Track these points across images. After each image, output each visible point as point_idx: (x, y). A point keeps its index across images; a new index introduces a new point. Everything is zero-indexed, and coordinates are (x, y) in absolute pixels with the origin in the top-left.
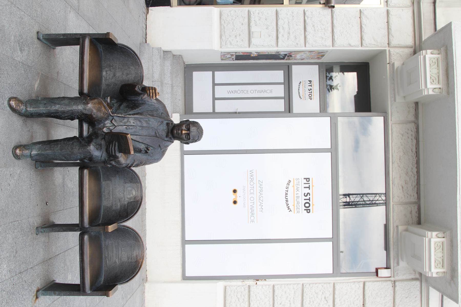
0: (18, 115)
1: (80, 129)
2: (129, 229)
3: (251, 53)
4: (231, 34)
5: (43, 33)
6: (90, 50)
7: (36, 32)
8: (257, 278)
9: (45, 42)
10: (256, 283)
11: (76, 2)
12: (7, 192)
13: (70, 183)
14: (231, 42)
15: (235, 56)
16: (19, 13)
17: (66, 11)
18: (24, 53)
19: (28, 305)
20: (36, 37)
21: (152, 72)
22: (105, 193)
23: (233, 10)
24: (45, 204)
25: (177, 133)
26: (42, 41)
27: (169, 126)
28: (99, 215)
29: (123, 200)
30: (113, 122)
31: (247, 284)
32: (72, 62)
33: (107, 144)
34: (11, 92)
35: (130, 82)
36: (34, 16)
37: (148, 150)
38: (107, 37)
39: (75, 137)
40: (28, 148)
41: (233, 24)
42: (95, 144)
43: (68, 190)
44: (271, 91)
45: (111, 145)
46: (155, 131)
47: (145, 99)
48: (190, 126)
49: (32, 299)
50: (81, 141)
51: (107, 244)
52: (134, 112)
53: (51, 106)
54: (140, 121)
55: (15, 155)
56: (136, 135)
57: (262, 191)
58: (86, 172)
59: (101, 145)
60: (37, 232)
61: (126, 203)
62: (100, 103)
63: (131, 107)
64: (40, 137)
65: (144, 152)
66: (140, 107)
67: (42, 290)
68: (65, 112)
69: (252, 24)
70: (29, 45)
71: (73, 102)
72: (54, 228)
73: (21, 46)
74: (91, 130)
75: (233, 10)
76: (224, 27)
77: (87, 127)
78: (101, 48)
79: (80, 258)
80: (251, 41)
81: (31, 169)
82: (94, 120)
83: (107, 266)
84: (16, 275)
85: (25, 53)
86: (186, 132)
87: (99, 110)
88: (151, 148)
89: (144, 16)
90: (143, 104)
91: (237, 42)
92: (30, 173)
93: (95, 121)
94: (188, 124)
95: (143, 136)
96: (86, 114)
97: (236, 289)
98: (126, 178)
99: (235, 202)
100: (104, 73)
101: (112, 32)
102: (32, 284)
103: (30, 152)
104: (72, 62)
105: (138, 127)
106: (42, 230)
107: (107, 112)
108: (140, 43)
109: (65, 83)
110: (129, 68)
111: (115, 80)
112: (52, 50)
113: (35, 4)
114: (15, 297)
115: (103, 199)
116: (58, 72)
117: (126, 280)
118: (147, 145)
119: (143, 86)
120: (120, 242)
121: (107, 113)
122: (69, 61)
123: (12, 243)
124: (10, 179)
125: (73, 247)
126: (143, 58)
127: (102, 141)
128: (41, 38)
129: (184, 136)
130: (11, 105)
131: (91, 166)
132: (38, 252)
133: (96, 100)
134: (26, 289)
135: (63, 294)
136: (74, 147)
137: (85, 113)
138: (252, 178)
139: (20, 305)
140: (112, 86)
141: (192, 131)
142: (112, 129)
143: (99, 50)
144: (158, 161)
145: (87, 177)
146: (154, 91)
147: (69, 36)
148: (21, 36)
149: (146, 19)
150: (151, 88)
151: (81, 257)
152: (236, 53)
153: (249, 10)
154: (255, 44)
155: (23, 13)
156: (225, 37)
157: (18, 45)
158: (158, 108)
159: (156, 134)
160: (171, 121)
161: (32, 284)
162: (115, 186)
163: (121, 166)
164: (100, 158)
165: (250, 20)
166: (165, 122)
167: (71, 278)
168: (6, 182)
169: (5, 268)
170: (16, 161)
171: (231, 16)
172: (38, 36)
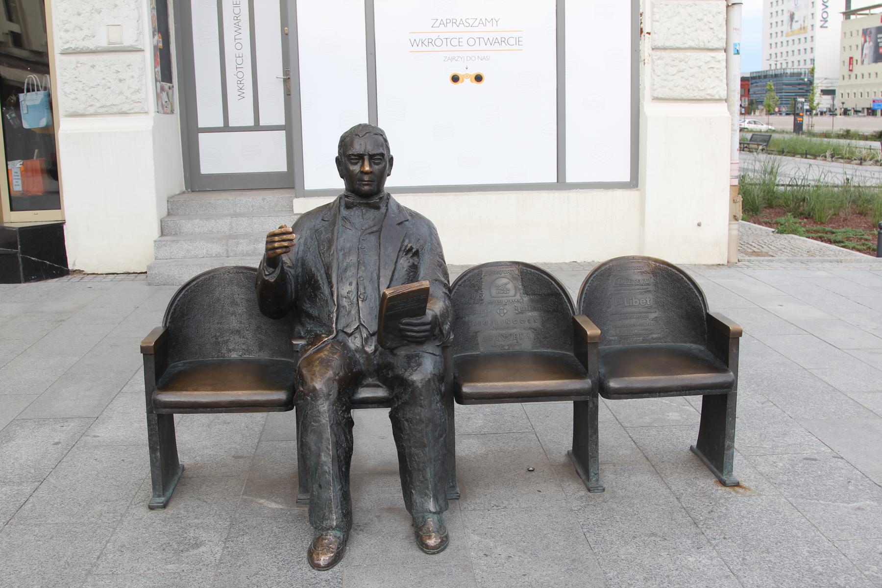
0: (347, 544)
1: (370, 406)
2: (585, 290)
3: (155, 47)
4: (117, 92)
5: (151, 495)
6: (186, 390)
7: (151, 513)
8: (638, 32)
9: (171, 490)
10: (648, 35)
11: (72, 424)
12: (526, 561)
13: (475, 421)
14: (135, 92)
15: (164, 83)
16: (112, 556)
17: (95, 446)
18: (203, 539)
19: (759, 505)
20: (162, 512)
21: (207, 257)
22: (505, 345)
23: (62, 89)
24: (533, 473)
25: (370, 183)
26: (170, 498)
27: (353, 203)
28: (556, 356)
29: (520, 305)
30: (351, 332)
31: (650, 53)
32: (209, 426)
33: (405, 342)
34: (298, 563)
35: (254, 296)
36: (115, 520)
37: (411, 249)
38: (153, 353)
39: (390, 416)
40: (421, 519)
41: (94, 87)
42: (409, 370)
43: (491, 424)
44: (236, 5)
45: (409, 334)
46: (367, 236)
47: (293, 258)
48: (353, 155)
49: (743, 495)
50: (402, 403)
51: (616, 338)
52: (325, 283)
53: (324, 472)
54: (345, 270)
55: (440, 547)
56: (379, 278)
57: (454, 21)
58: (467, 389)
59: (408, 357)
60: (598, 490)
61: (526, 299)
62: (310, 362)
63: (313, 292)
64: (393, 491)
65: (416, 258)
66: (313, 270)
67: (719, 474)
68: (337, 441)
69: (91, 44)
70: (182, 527)
71: (313, 423)
72: (590, 454)
73: (186, 546)
74: (370, 380)
75: (63, 88)
76: (102, 107)
77: (365, 389)
78: (176, 365)
79: (660, 396)
80: (128, 47)
81: (462, 508)
82: (350, 374)
83: (664, 337)
84: (703, 534)
85: (203, 536)
86: (366, 163)
87: (326, 363)
88: (406, 243)
89: (87, 278)
90: (303, 264)
91: (132, 77)
92: (473, 511)
93: (351, 372)
94: (346, 159)
95: (379, 262)
96: (339, 393)
97: (658, 76)
98: (471, 298)
99: (479, 78)
100: (233, 356)
101: (140, 341)
102: (712, 496)
103: (430, 515)
104: (209, 427)
105: (361, 273)
106: (594, 479)
107: (330, 346)
108: (147, 285)
109: (257, 441)
110: (219, 300)
111: (247, 330)
112: (186, 473)
113: (86, 517)
114: (750, 535)
115: (517, 348)
116: (233, 457)
117: (698, 295)
118: (401, 253)
119: (265, 264)
120: (611, 309)
121: (332, 346)
122: (207, 434)
123: (638, 545)
124: (496, 556)
125: (610, 410)
126: (179, 278)
127: (398, 353)
128: (162, 499)
129: (376, 167)
130: (329, 563)
131: (453, 377)
132: (640, 485)
133: (304, 371)
134: (727, 509)
135: (732, 430)
136: (418, 417)
137: (336, 396)
138: (426, 42)
139: (765, 522)
140: (263, 337)
141: (363, 150)
142: (368, 333)
143: (183, 368)
144: (434, 229)
145: (479, 384)
146: (276, 238)
147: (155, 439)
148: (164, 546)
149: (95, 276)
150: (268, 246)
151: (657, 394)
152: (156, 81)
153: (61, 53)
154: (136, 39)
155: (108, 544)
156: (124, 103)
157: (186, 554)
158: (311, 229)
159: (372, 232)
160: (340, 200)
161: (712, 496)
162: (490, 322)
163: (450, 310)
164: (438, 357)
165: (82, 49)
166: (344, 212)
167: (677, 414)
168: (505, 564)
169: (695, 559)
170: (453, 543)
171: (76, 92)
172: (158, 507)
